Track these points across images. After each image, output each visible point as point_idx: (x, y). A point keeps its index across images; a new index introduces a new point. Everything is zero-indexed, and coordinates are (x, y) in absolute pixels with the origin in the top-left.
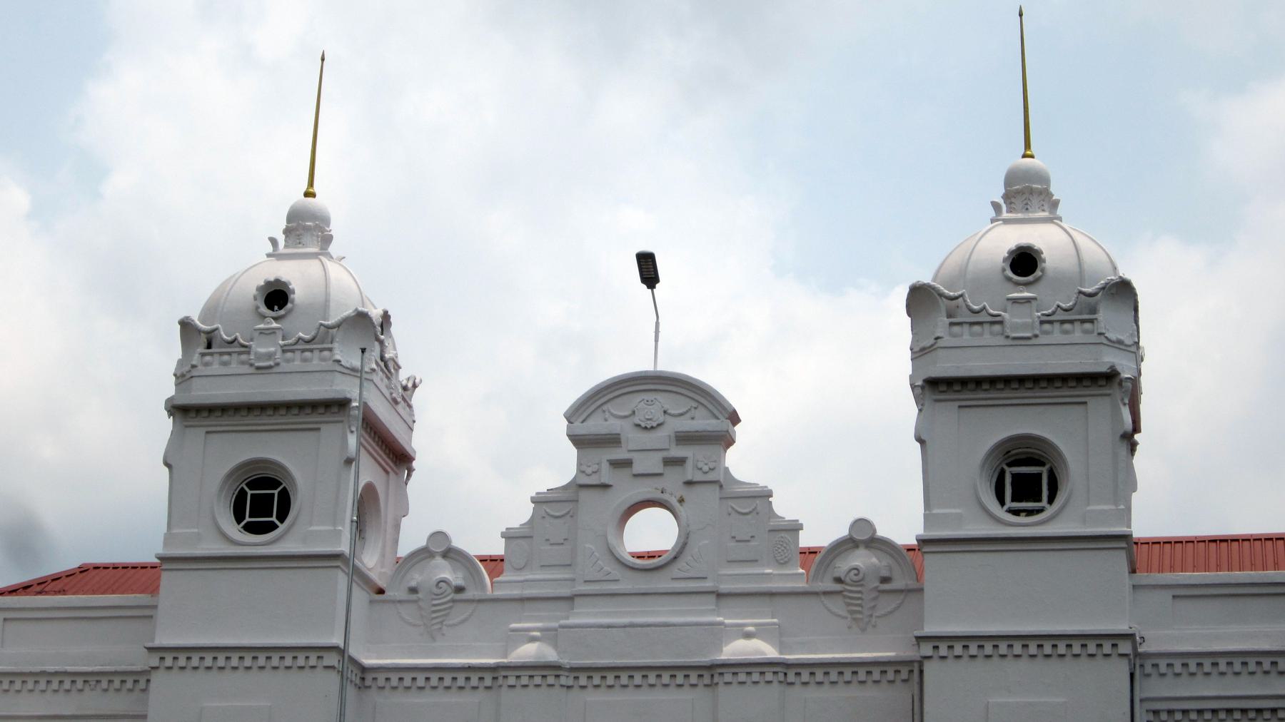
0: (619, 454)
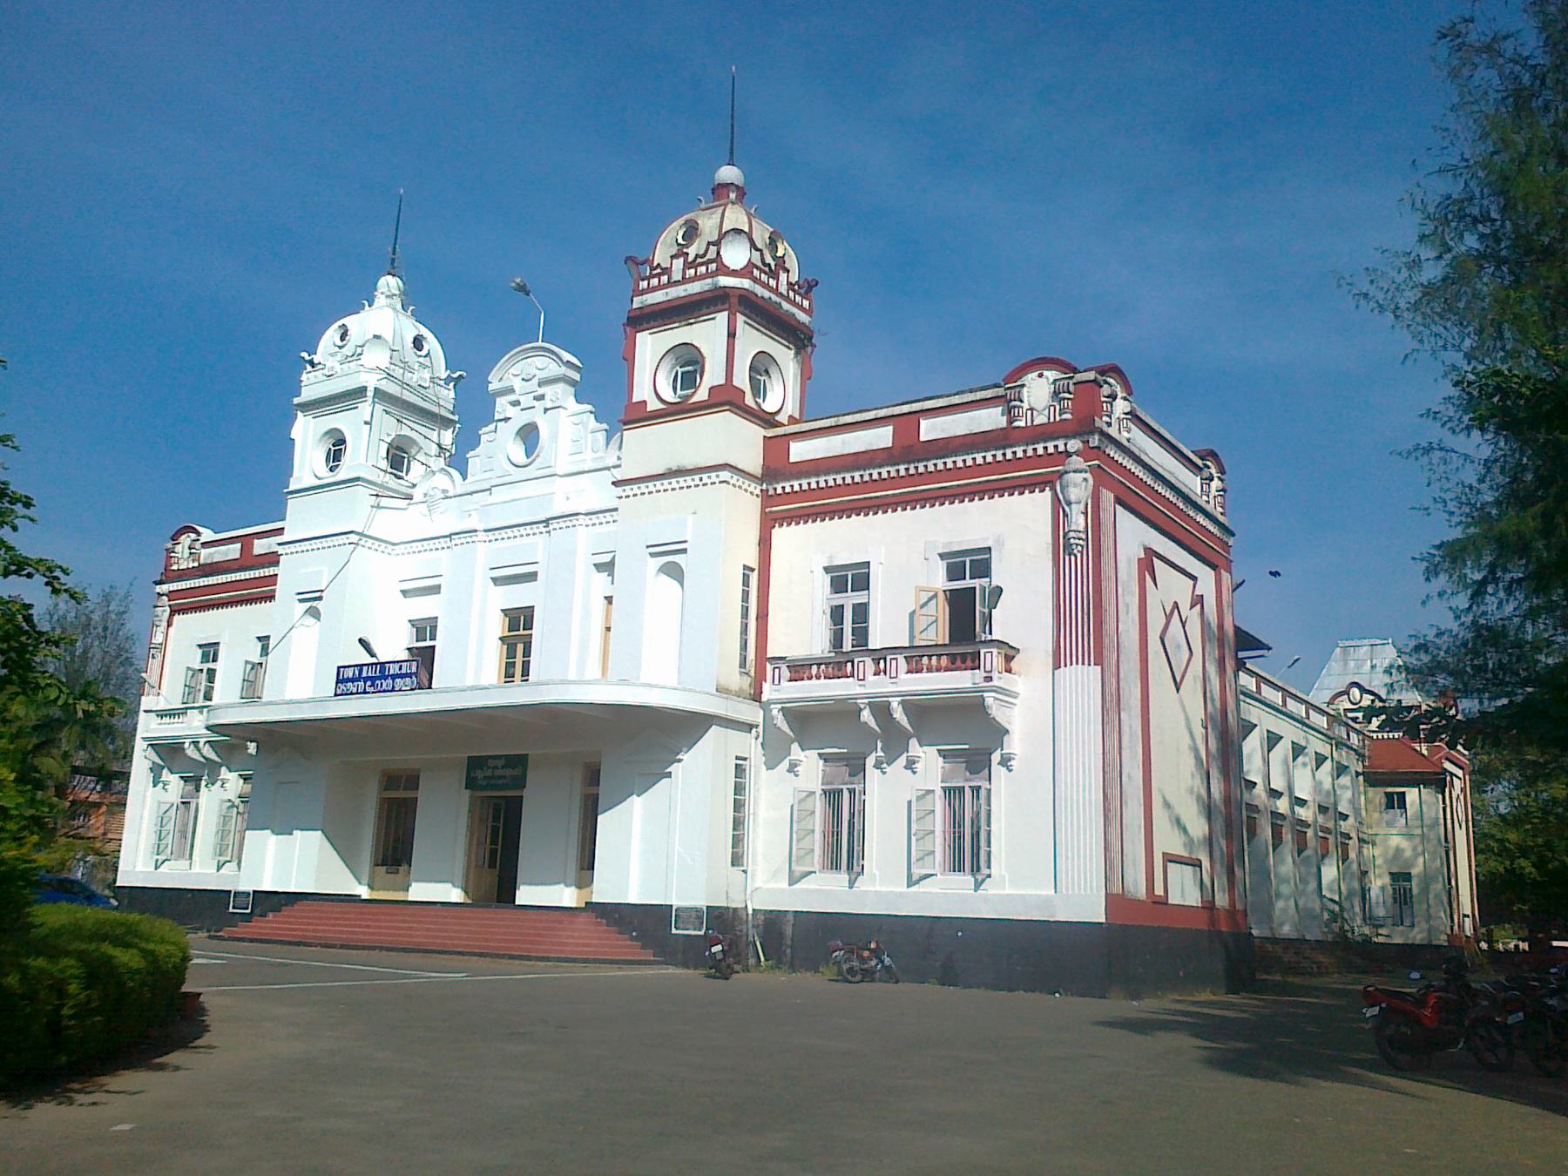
0: (512, 398)
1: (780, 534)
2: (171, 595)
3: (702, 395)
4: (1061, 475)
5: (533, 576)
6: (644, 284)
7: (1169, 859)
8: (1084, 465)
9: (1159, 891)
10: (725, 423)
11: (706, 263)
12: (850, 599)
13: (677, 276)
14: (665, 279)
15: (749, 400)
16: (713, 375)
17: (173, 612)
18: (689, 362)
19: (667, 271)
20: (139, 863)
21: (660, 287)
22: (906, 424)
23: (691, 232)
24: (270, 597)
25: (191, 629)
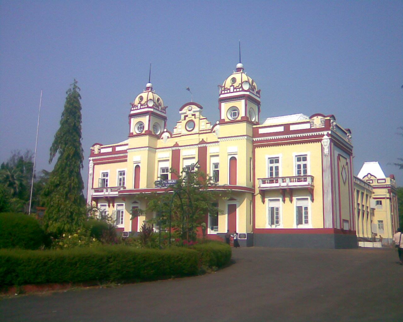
1: (257, 150)
2: (93, 160)
3: (144, 132)
4: (322, 140)
5: (218, 156)
6: (132, 109)
7: (344, 220)
8: (328, 138)
9: (342, 227)
10: (244, 125)
11: (239, 88)
12: (274, 165)
13: (232, 91)
14: (228, 91)
15: (153, 133)
16: (146, 128)
17: (95, 164)
18: (234, 111)
19: (229, 89)
20: (209, 233)
21: (227, 93)
22: (114, 148)
23: (234, 80)
24: (126, 161)
25: (100, 170)
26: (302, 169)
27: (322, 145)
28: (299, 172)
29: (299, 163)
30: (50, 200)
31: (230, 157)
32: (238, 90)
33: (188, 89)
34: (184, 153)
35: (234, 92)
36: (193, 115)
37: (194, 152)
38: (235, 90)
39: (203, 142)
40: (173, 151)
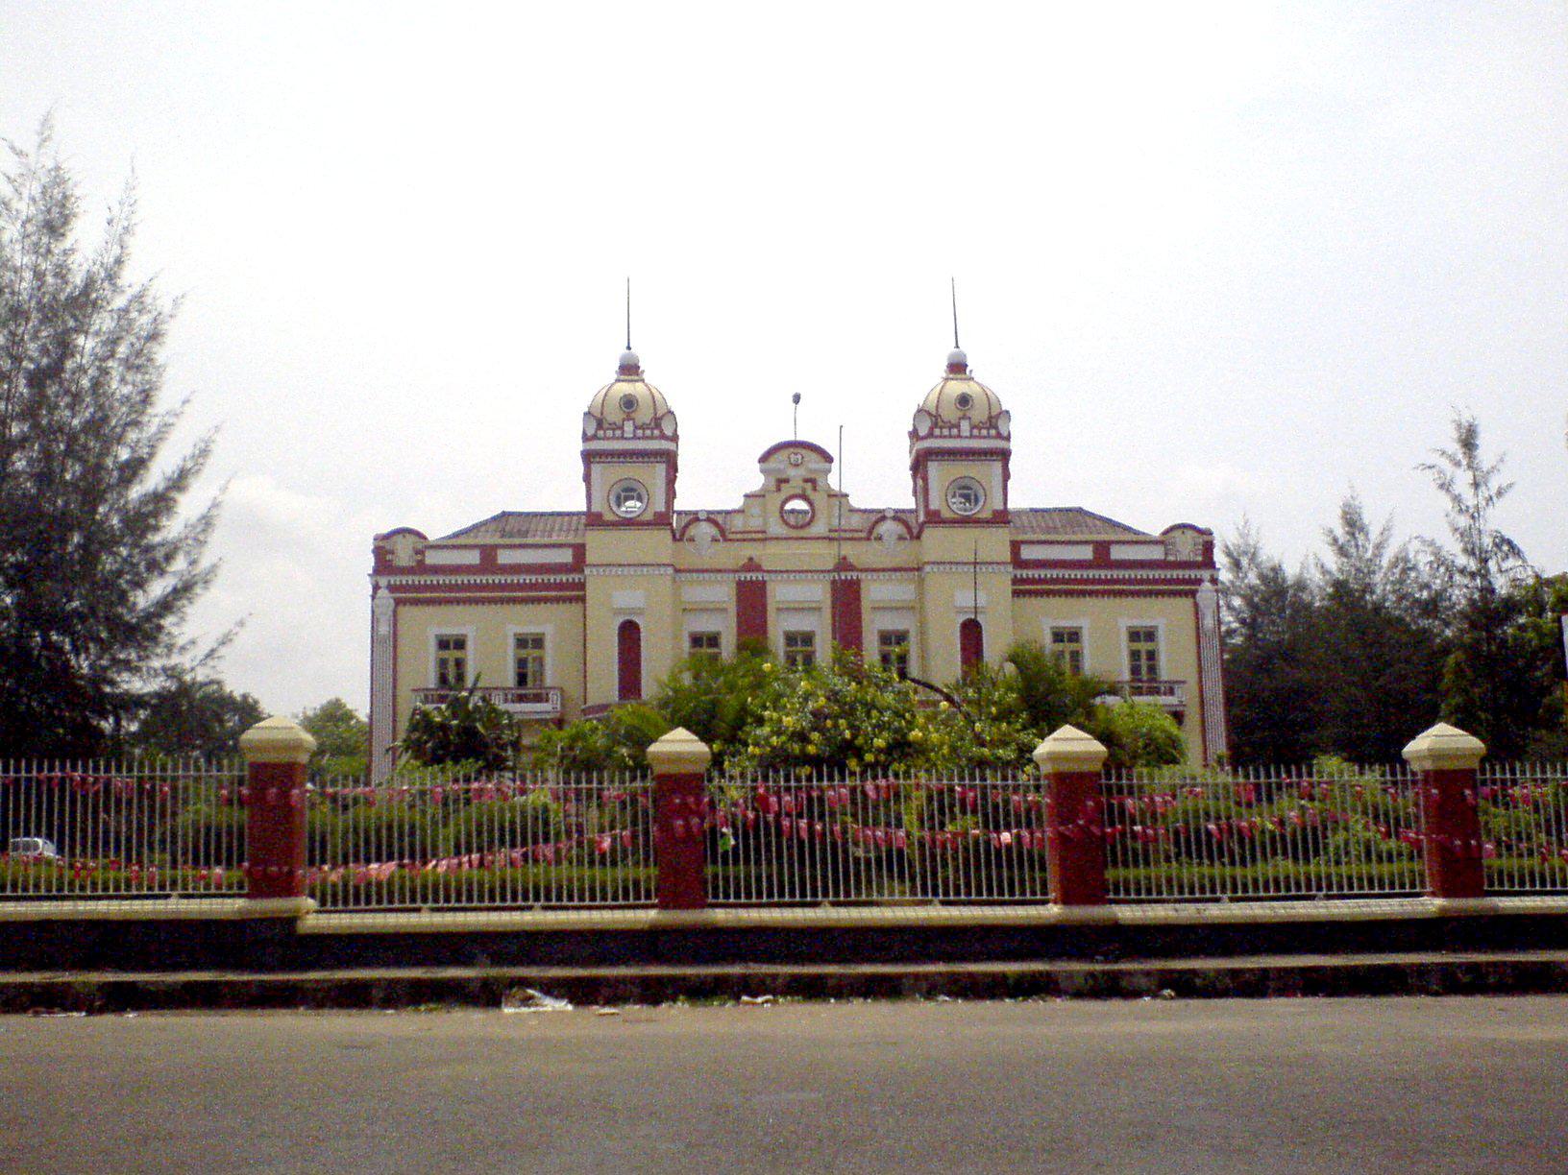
17: (398, 602)
21: (614, 438)
26: (1144, 663)
27: (1196, 605)
28: (1135, 671)
29: (523, 653)
30: (811, 749)
31: (621, 619)
32: (648, 432)
33: (797, 399)
34: (779, 593)
35: (635, 437)
36: (806, 481)
37: (819, 592)
38: (640, 432)
39: (752, 566)
40: (740, 584)
